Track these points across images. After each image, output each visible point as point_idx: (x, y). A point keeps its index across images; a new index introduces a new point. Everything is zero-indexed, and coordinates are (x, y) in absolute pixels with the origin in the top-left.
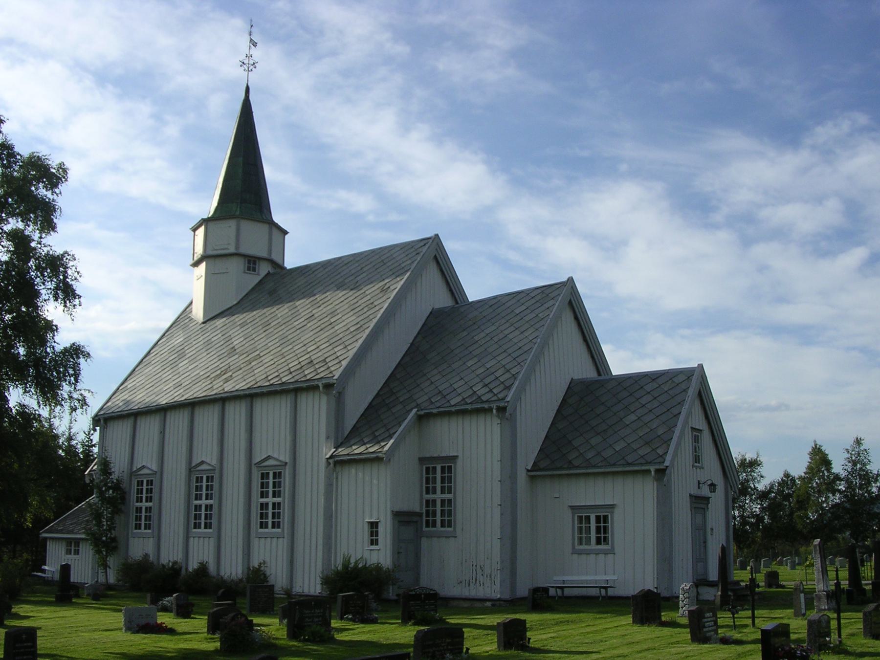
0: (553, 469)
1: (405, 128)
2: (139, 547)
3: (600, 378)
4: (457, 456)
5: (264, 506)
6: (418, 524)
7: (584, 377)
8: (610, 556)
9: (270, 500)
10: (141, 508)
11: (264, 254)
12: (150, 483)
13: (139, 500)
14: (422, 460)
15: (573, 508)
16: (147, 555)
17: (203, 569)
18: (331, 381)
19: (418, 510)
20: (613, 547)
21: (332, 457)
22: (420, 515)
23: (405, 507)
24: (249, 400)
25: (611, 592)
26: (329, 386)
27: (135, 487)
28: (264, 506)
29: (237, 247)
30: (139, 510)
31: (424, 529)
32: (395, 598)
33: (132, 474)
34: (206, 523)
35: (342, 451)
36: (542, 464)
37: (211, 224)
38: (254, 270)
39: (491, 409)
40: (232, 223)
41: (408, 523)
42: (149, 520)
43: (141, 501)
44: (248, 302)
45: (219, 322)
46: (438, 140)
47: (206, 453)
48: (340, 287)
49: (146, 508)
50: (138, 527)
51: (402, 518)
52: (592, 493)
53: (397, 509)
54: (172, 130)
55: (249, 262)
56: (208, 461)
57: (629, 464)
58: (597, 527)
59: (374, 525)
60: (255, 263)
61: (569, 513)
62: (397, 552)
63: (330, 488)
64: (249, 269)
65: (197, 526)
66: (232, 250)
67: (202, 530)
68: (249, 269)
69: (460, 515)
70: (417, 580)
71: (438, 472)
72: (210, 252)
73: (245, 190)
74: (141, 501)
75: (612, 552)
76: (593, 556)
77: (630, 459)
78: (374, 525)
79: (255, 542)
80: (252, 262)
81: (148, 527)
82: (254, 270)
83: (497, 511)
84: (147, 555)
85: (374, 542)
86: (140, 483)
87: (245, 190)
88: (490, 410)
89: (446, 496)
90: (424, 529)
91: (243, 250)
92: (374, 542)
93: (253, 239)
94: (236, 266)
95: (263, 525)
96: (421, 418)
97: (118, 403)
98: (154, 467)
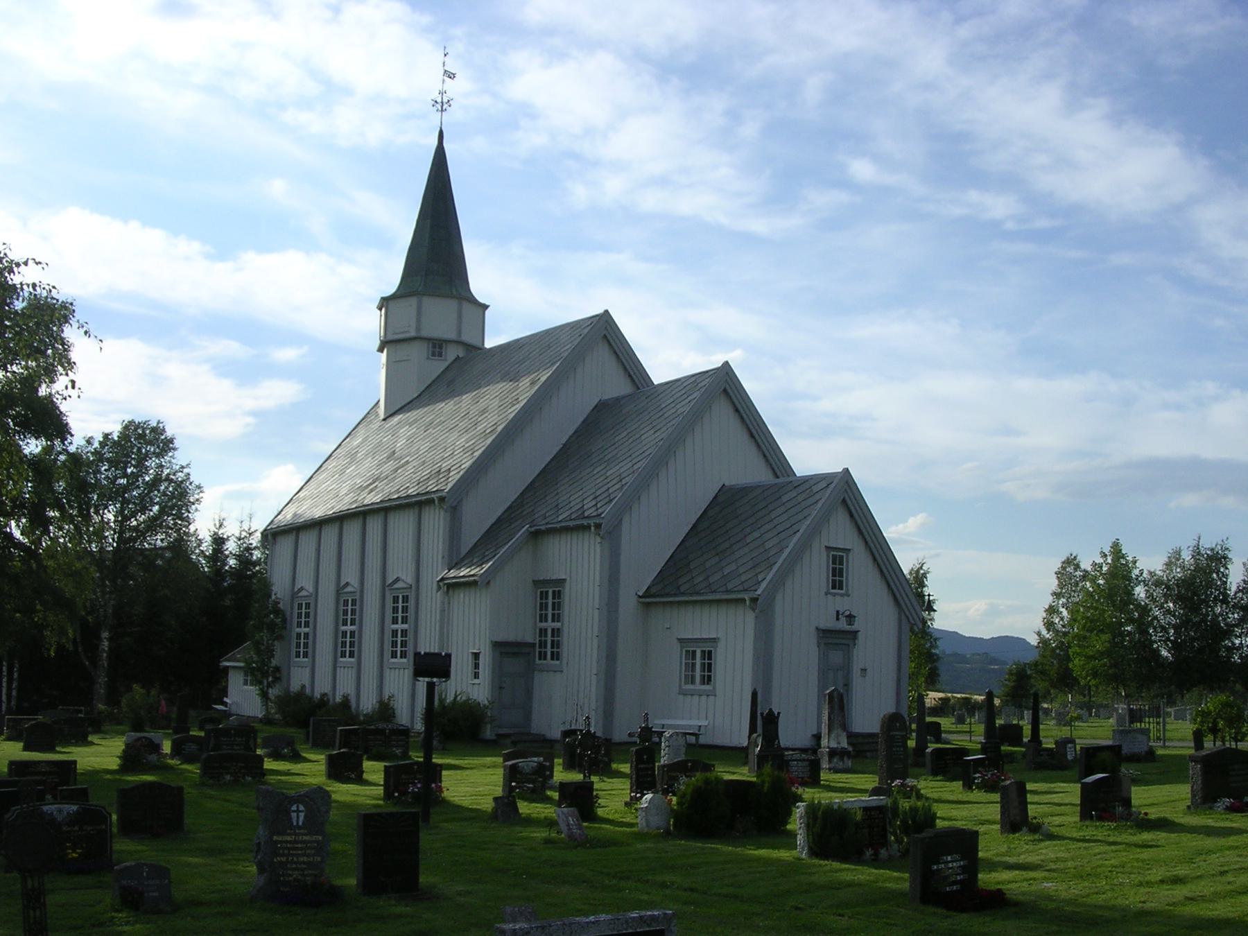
0: (662, 596)
1: (1075, 99)
2: (298, 678)
3: (777, 481)
4: (565, 580)
5: (395, 633)
6: (521, 657)
7: (733, 483)
8: (712, 698)
9: (550, 625)
10: (546, 630)
11: (452, 335)
12: (308, 605)
13: (299, 625)
14: (536, 583)
15: (680, 640)
16: (303, 687)
17: (346, 703)
18: (444, 494)
19: (530, 640)
20: (714, 688)
21: (442, 579)
22: (533, 645)
23: (511, 637)
24: (383, 513)
25: (702, 740)
26: (442, 499)
27: (296, 611)
28: (395, 633)
29: (418, 329)
30: (299, 635)
31: (538, 662)
32: (494, 737)
33: (294, 595)
34: (552, 653)
35: (453, 573)
36: (653, 591)
37: (391, 304)
38: (440, 355)
39: (589, 527)
40: (413, 301)
41: (515, 654)
42: (307, 648)
43: (546, 621)
44: (431, 393)
45: (396, 419)
46: (1116, 119)
47: (401, 570)
48: (502, 379)
49: (553, 630)
50: (298, 655)
51: (504, 649)
52: (698, 623)
53: (501, 637)
54: (750, 130)
55: (434, 347)
56: (404, 578)
57: (728, 591)
58: (701, 663)
59: (476, 656)
60: (441, 347)
61: (677, 646)
62: (498, 687)
63: (445, 612)
64: (433, 355)
65: (343, 655)
66: (413, 334)
67: (301, 659)
68: (433, 355)
69: (565, 650)
70: (528, 716)
71: (549, 595)
72: (390, 337)
73: (436, 253)
74: (546, 621)
75: (712, 693)
76: (696, 698)
77: (730, 586)
78: (476, 656)
79: (387, 673)
80: (437, 346)
81: (306, 655)
82: (440, 355)
83: (595, 641)
84: (303, 687)
85: (476, 676)
86: (300, 606)
87: (436, 253)
88: (589, 527)
89: (557, 625)
90: (538, 662)
91: (424, 334)
92: (476, 676)
93: (439, 317)
94: (417, 352)
95: (394, 655)
96: (536, 535)
97: (287, 517)
98: (311, 590)
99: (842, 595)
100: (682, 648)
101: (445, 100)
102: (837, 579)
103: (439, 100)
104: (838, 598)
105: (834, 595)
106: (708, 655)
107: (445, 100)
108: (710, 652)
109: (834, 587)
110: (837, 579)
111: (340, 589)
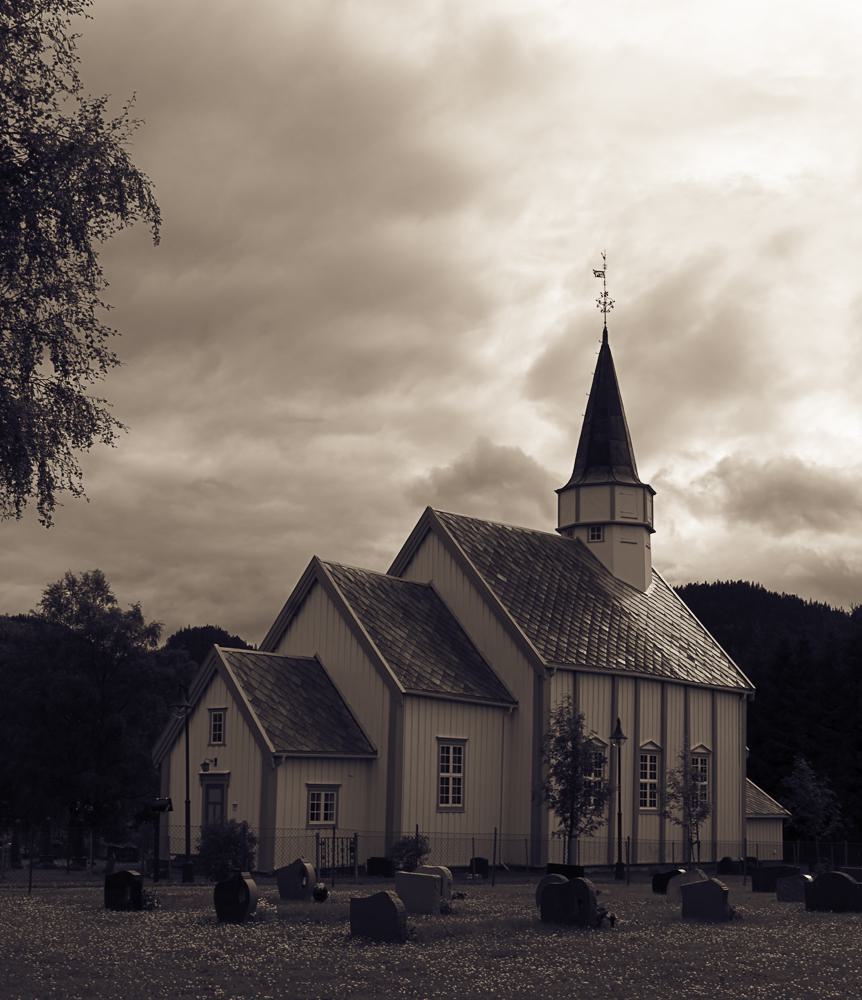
9: (451, 775)
11: (607, 519)
15: (307, 785)
55: (593, 531)
60: (599, 530)
82: (599, 538)
91: (583, 520)
99: (219, 745)
100: (309, 791)
101: (608, 301)
102: (218, 734)
103: (602, 300)
104: (216, 748)
105: (214, 746)
106: (458, 751)
107: (608, 301)
108: (460, 749)
109: (214, 740)
110: (218, 734)
111: (687, 756)
